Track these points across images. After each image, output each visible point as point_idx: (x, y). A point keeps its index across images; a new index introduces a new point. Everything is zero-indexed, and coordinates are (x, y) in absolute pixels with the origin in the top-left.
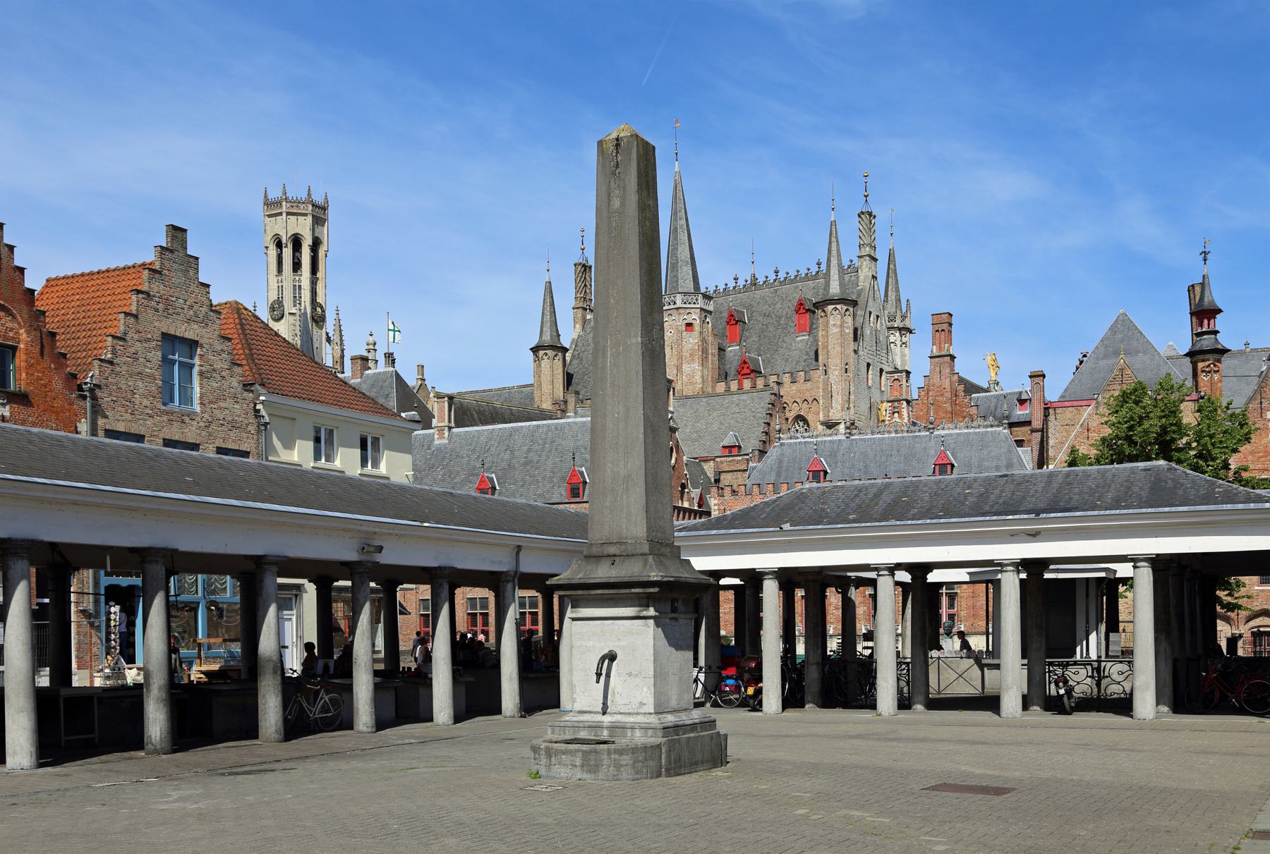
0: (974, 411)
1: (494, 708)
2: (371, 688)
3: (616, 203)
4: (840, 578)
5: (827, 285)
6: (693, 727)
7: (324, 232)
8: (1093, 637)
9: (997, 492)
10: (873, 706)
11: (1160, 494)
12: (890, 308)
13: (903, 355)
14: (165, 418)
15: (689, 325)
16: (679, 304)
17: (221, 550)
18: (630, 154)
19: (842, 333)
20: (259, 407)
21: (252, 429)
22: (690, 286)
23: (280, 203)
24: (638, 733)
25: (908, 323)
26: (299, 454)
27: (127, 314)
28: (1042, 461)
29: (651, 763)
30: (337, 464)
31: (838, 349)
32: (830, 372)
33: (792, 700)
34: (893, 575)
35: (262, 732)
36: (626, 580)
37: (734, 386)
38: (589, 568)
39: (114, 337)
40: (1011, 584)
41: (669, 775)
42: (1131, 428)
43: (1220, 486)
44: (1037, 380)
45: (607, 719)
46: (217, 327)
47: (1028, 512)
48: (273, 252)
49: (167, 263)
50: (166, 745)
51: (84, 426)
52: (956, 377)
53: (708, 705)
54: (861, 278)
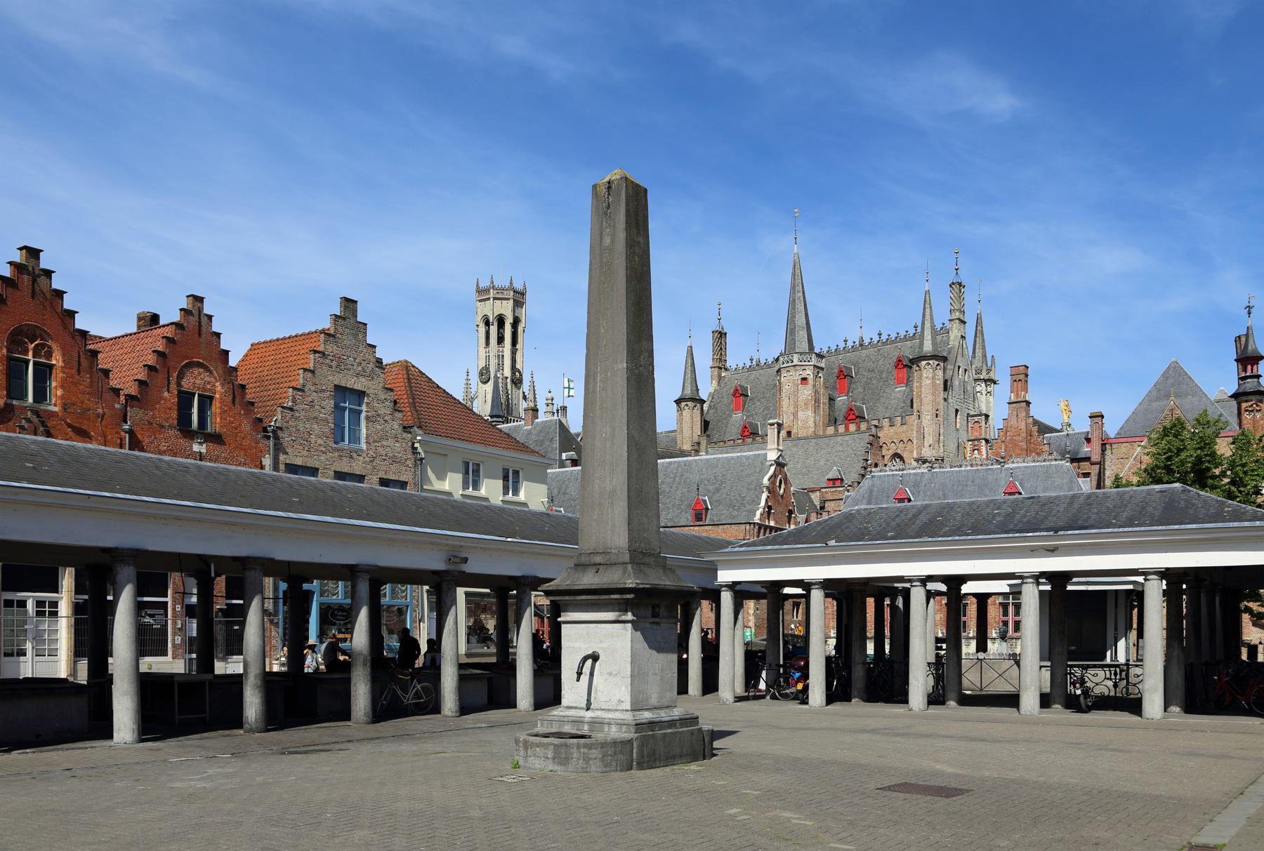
0: (1046, 448)
1: (509, 701)
2: (456, 679)
3: (607, 240)
4: (884, 589)
5: (921, 344)
6: (671, 724)
7: (522, 313)
8: (1121, 644)
9: (1023, 512)
10: (906, 702)
11: (1172, 513)
12: (977, 363)
13: (988, 402)
15: (804, 379)
16: (796, 362)
17: (316, 560)
18: (619, 194)
19: (934, 384)
21: (410, 463)
22: (805, 347)
24: (614, 728)
25: (992, 375)
26: (451, 484)
27: (305, 370)
30: (483, 492)
31: (930, 397)
32: (923, 417)
33: (832, 697)
34: (925, 586)
35: (354, 714)
37: (841, 429)
39: (294, 388)
40: (1031, 597)
41: (641, 766)
42: (1169, 459)
43: (1229, 506)
44: (1096, 420)
46: (381, 380)
47: (1047, 530)
48: (482, 329)
51: (267, 461)
52: (1031, 420)
54: (952, 338)
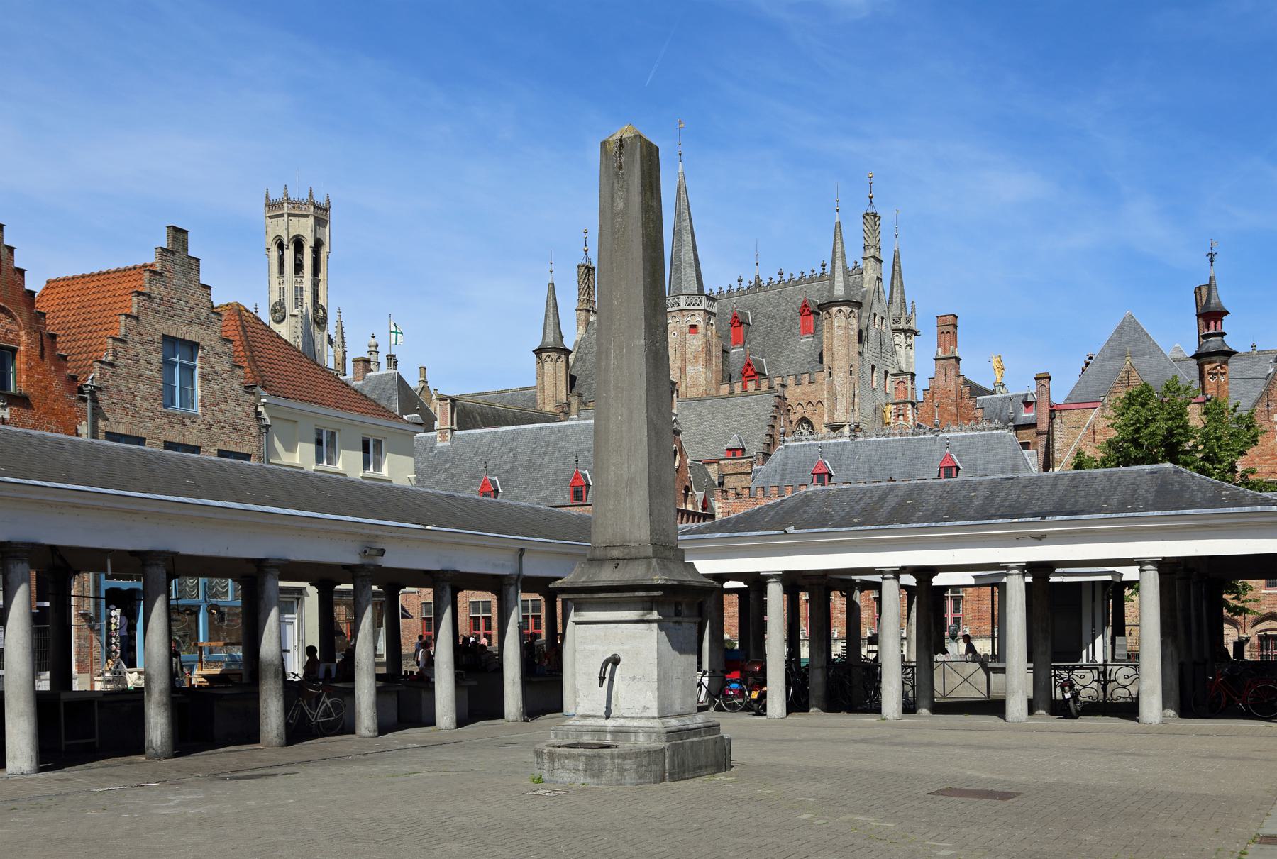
0: (979, 413)
1: (497, 712)
2: (373, 692)
3: (620, 204)
4: (845, 582)
5: (832, 287)
6: (697, 731)
7: (325, 234)
8: (1099, 641)
9: (1002, 495)
10: (878, 711)
11: (1166, 497)
12: (895, 310)
13: (908, 357)
14: (166, 421)
15: (693, 327)
16: (683, 306)
17: (223, 554)
18: (633, 155)
19: (847, 335)
20: (261, 409)
21: (253, 431)
22: (694, 288)
23: (282, 204)
24: (641, 737)
25: (913, 325)
26: (301, 457)
27: (127, 316)
28: (1047, 464)
29: (655, 768)
30: (339, 466)
31: (843, 351)
32: (834, 374)
33: (796, 704)
34: (898, 578)
35: (263, 736)
36: (630, 583)
37: (738, 388)
38: (592, 571)
39: (115, 339)
40: (1016, 588)
41: (673, 779)
42: (1137, 431)
43: (1226, 489)
44: (1043, 382)
45: (610, 723)
46: (218, 329)
47: (1034, 515)
48: (274, 253)
49: (167, 265)
50: (167, 749)
51: (84, 429)
52: (961, 379)
53: (712, 709)
54: (866, 279)
